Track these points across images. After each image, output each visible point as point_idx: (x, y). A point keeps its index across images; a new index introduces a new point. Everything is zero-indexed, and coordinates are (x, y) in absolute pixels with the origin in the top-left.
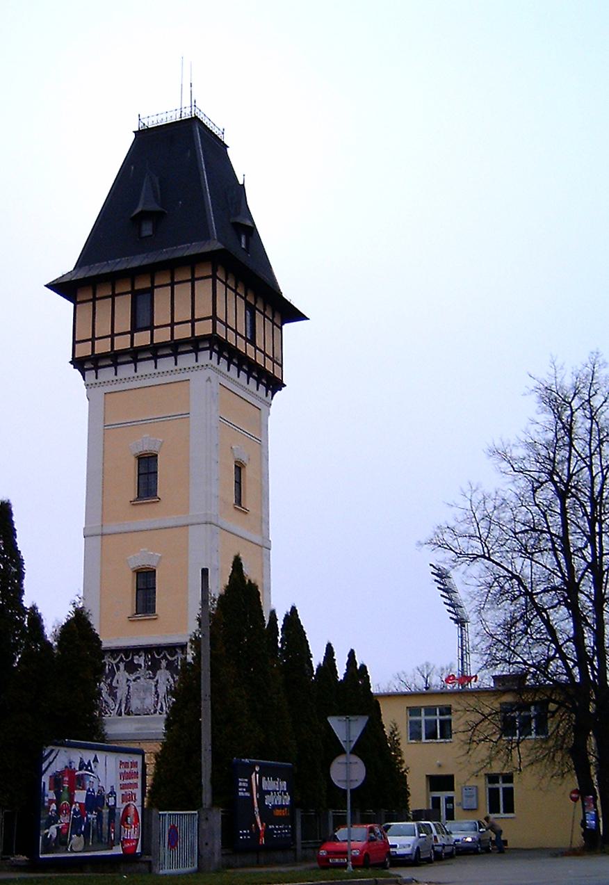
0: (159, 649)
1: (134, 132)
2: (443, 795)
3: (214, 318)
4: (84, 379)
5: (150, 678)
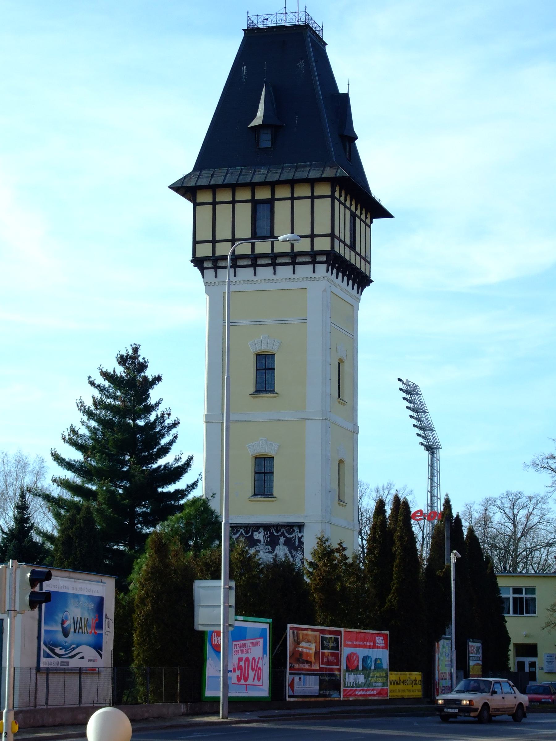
0: (278, 527)
1: (243, 30)
2: (527, 660)
3: (332, 235)
4: (203, 277)
5: (269, 552)
